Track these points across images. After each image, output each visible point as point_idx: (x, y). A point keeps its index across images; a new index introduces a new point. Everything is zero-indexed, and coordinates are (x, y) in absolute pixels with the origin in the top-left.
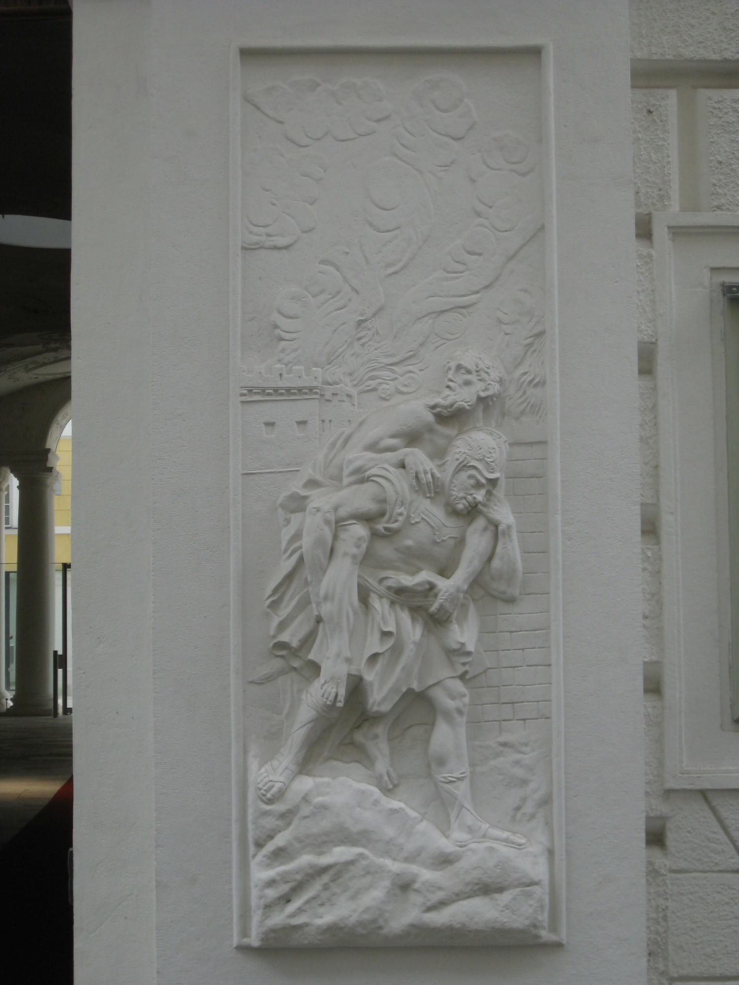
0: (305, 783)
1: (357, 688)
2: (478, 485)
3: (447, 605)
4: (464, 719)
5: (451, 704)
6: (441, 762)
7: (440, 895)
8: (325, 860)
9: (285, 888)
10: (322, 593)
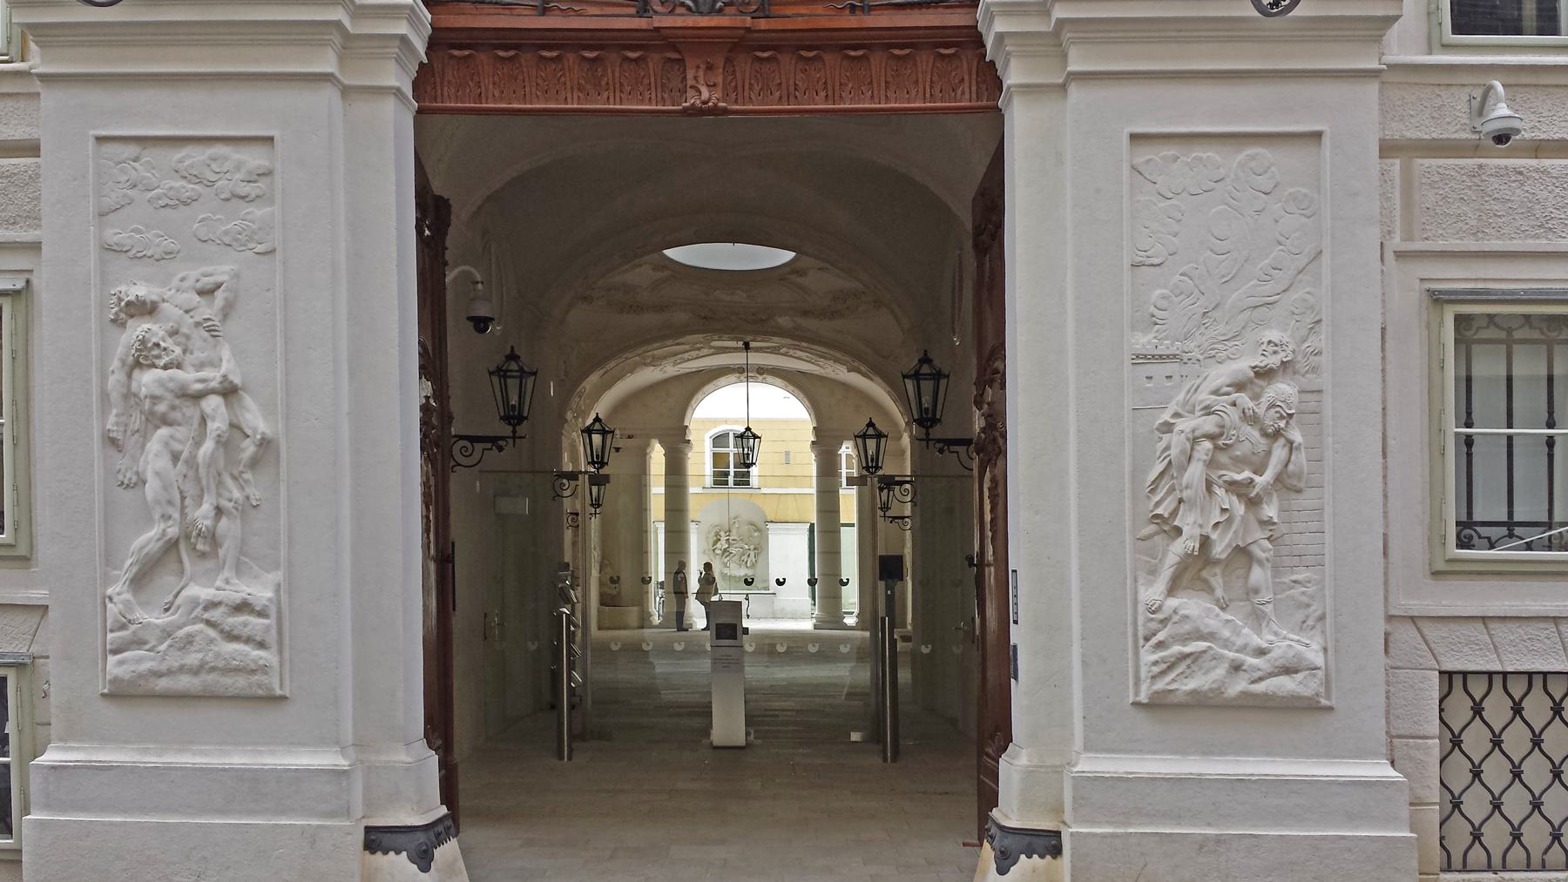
0: (1173, 602)
1: (1205, 542)
2: (1282, 417)
5: (1262, 555)
6: (1256, 591)
7: (1259, 674)
8: (1187, 650)
9: (1164, 666)
10: (1184, 482)
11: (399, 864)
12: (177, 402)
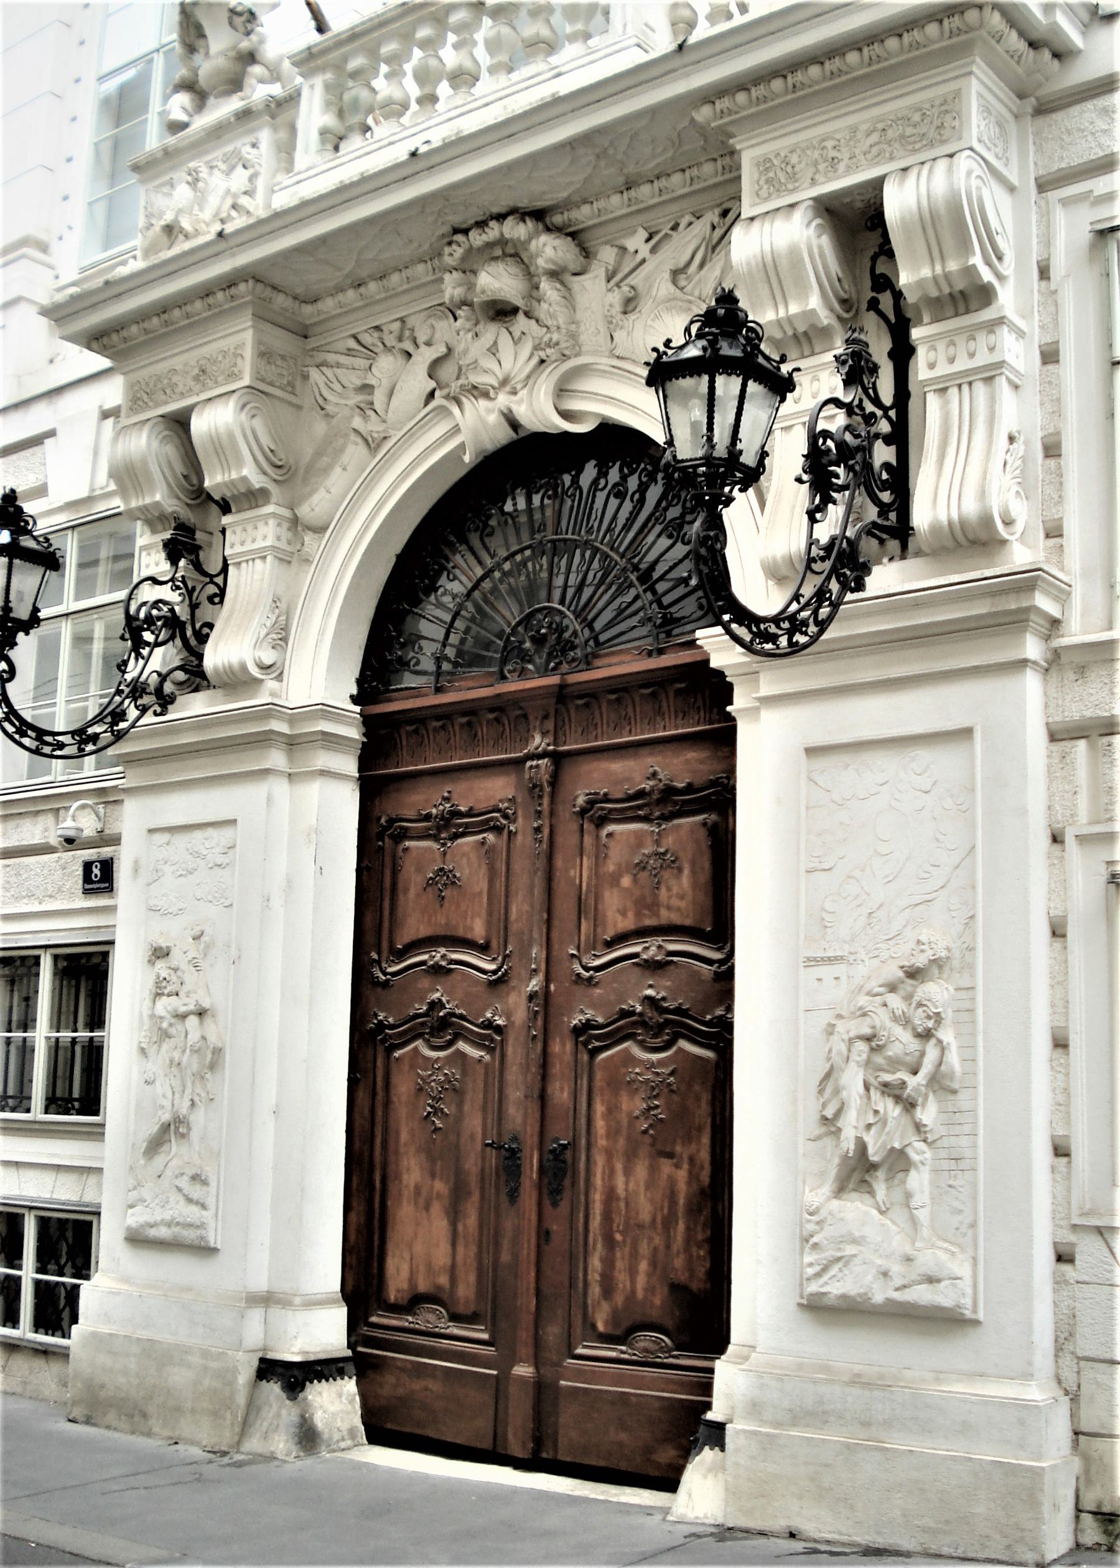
0: (835, 1204)
1: (862, 1147)
2: (929, 1017)
4: (927, 1168)
9: (817, 1268)
11: (273, 1389)
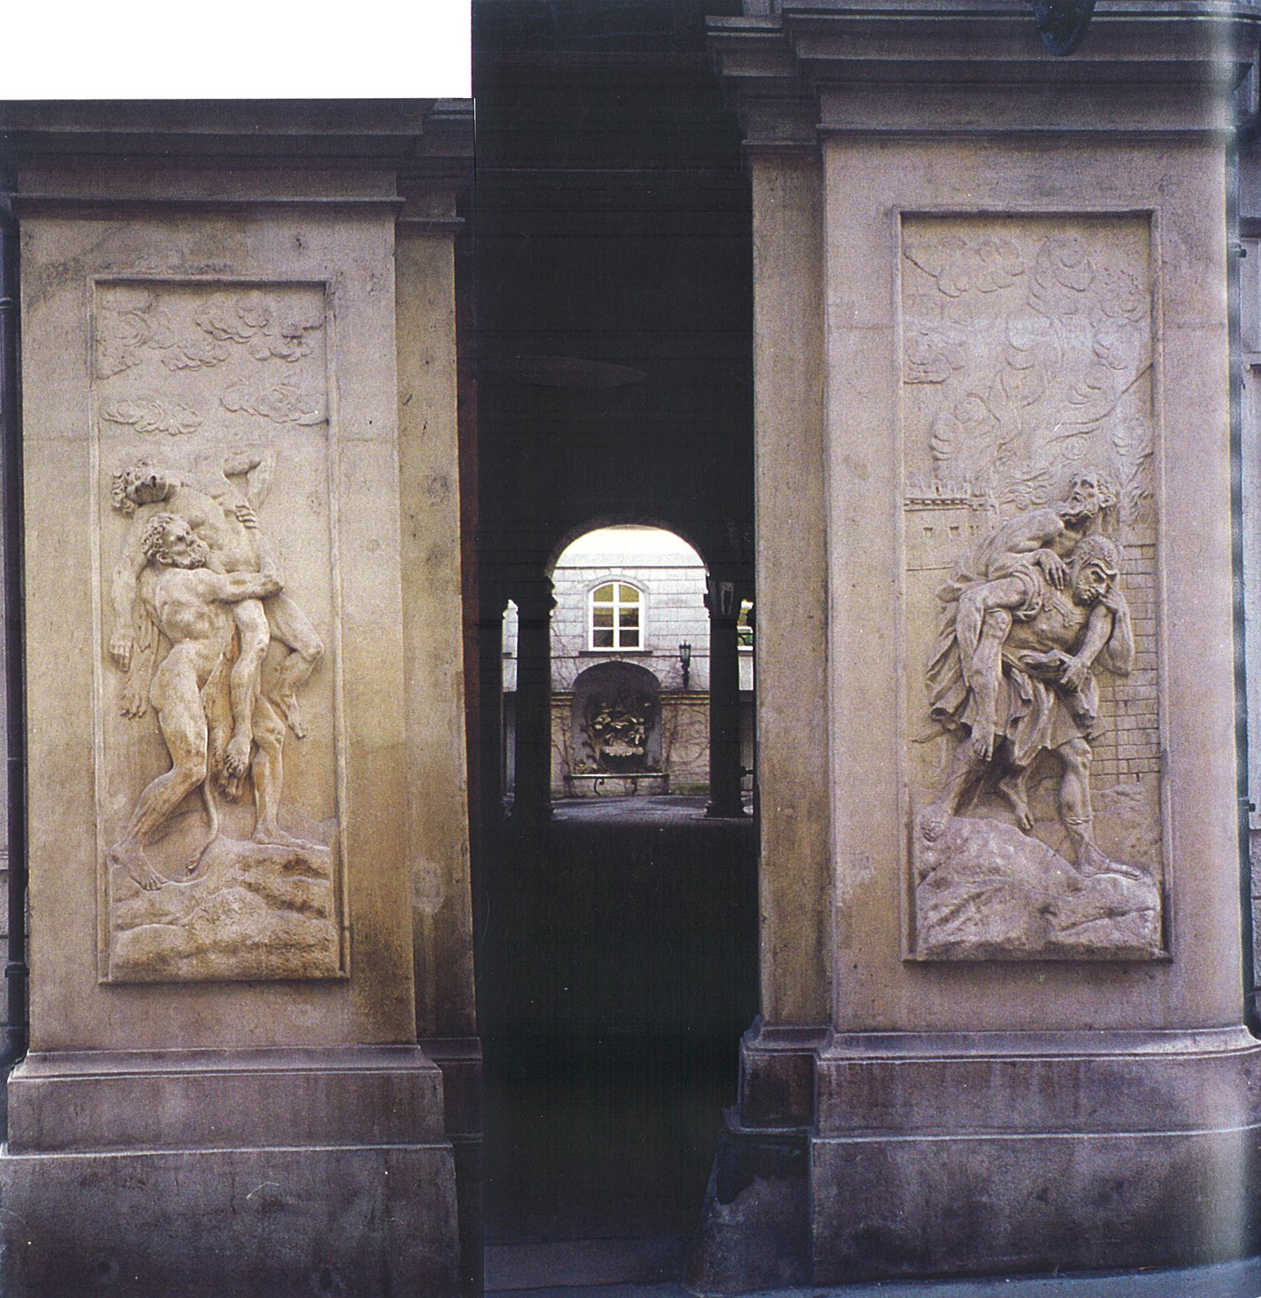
1: (1003, 746)
2: (1100, 580)
3: (1074, 678)
12: (206, 609)
